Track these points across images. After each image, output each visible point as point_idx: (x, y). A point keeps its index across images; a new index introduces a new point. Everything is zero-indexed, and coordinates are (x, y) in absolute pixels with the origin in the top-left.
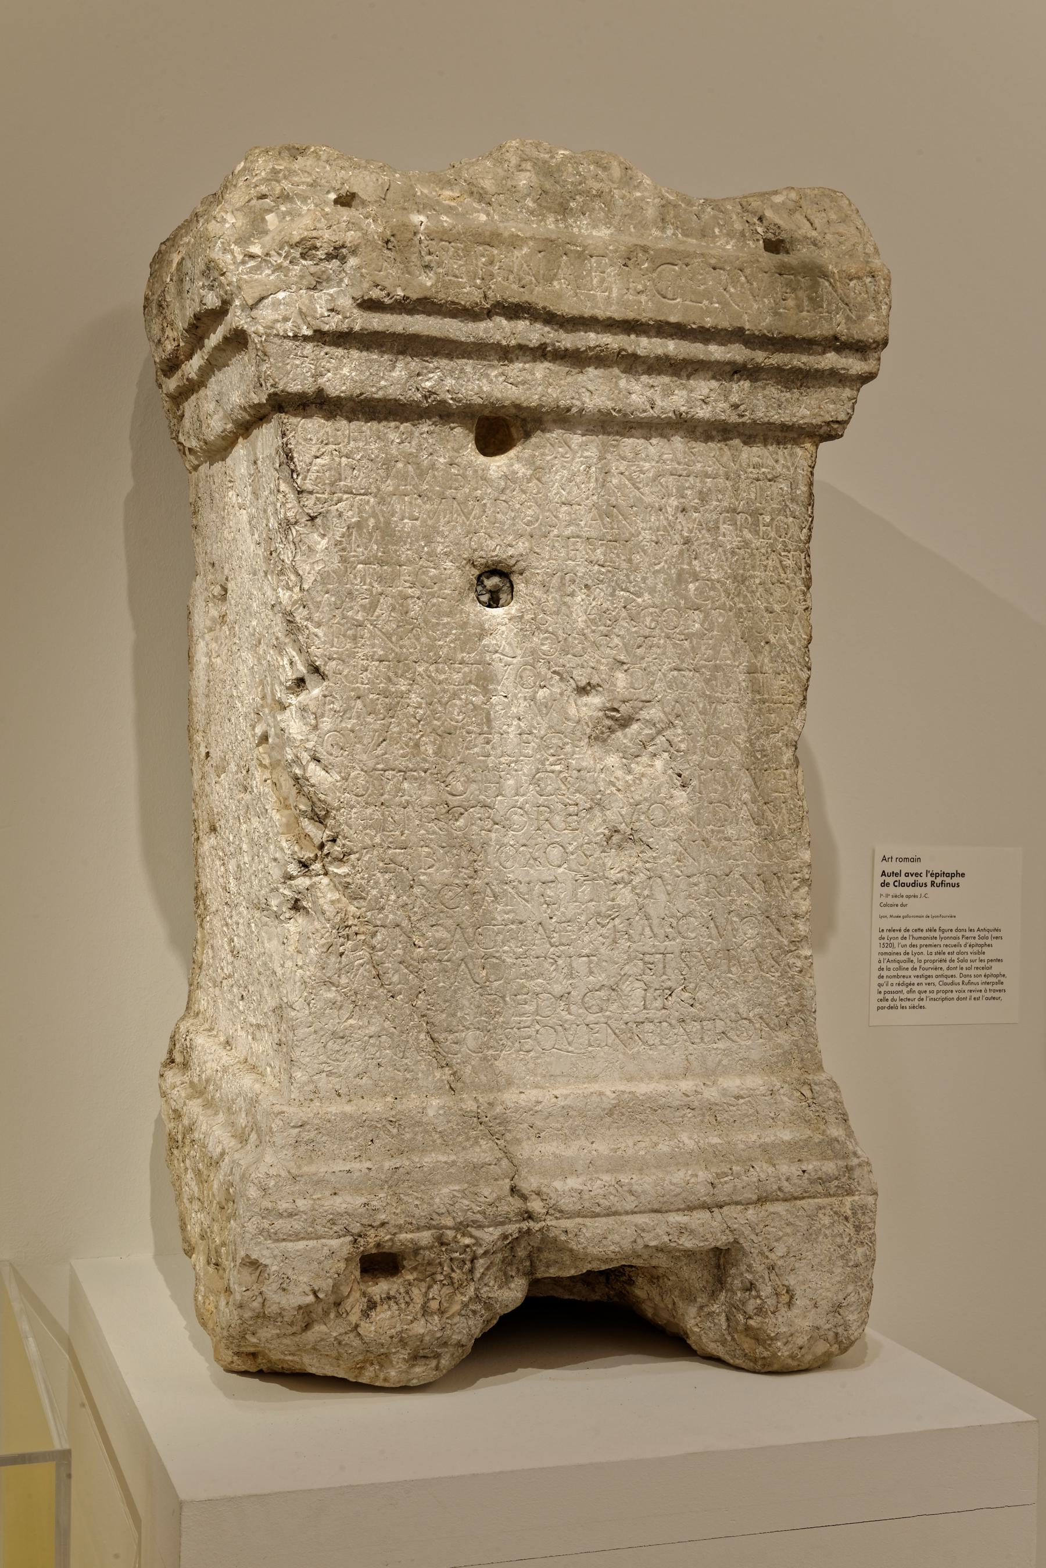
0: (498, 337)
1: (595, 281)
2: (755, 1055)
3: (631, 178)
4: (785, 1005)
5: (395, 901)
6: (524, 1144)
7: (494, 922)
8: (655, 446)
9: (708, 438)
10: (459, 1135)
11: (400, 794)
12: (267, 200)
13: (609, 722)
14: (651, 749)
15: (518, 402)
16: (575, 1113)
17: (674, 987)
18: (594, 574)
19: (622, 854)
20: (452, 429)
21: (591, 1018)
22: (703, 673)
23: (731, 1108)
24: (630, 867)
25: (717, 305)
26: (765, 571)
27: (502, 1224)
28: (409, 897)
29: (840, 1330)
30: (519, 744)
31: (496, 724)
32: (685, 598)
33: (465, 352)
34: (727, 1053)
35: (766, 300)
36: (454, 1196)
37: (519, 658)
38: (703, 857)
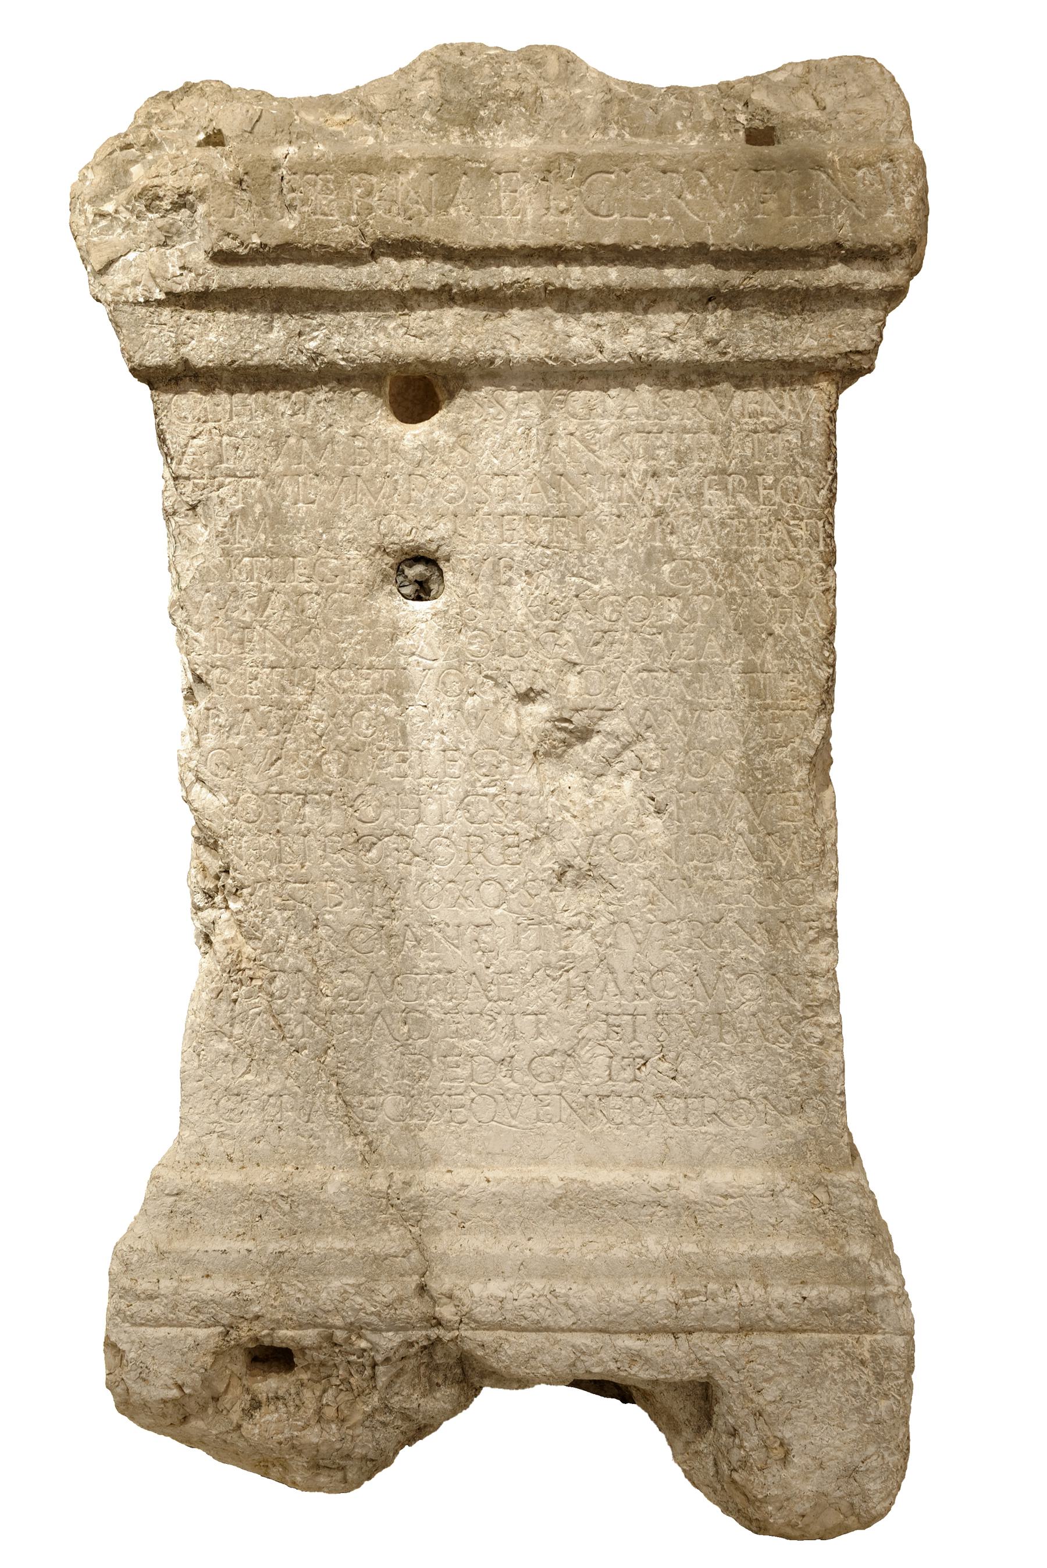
0: (386, 282)
1: (504, 203)
2: (756, 1143)
3: (572, 73)
5: (295, 943)
6: (443, 1234)
7: (416, 970)
8: (614, 399)
9: (685, 384)
10: (364, 1217)
13: (562, 735)
14: (618, 767)
15: (424, 357)
18: (537, 558)
20: (355, 394)
21: (540, 1088)
22: (682, 674)
23: (717, 1209)
24: (589, 909)
25: (668, 218)
26: (768, 545)
27: (404, 1329)
29: (856, 1500)
31: (413, 739)
32: (657, 583)
33: (352, 303)
34: (718, 1138)
35: (737, 206)
36: (346, 1292)
37: (441, 661)
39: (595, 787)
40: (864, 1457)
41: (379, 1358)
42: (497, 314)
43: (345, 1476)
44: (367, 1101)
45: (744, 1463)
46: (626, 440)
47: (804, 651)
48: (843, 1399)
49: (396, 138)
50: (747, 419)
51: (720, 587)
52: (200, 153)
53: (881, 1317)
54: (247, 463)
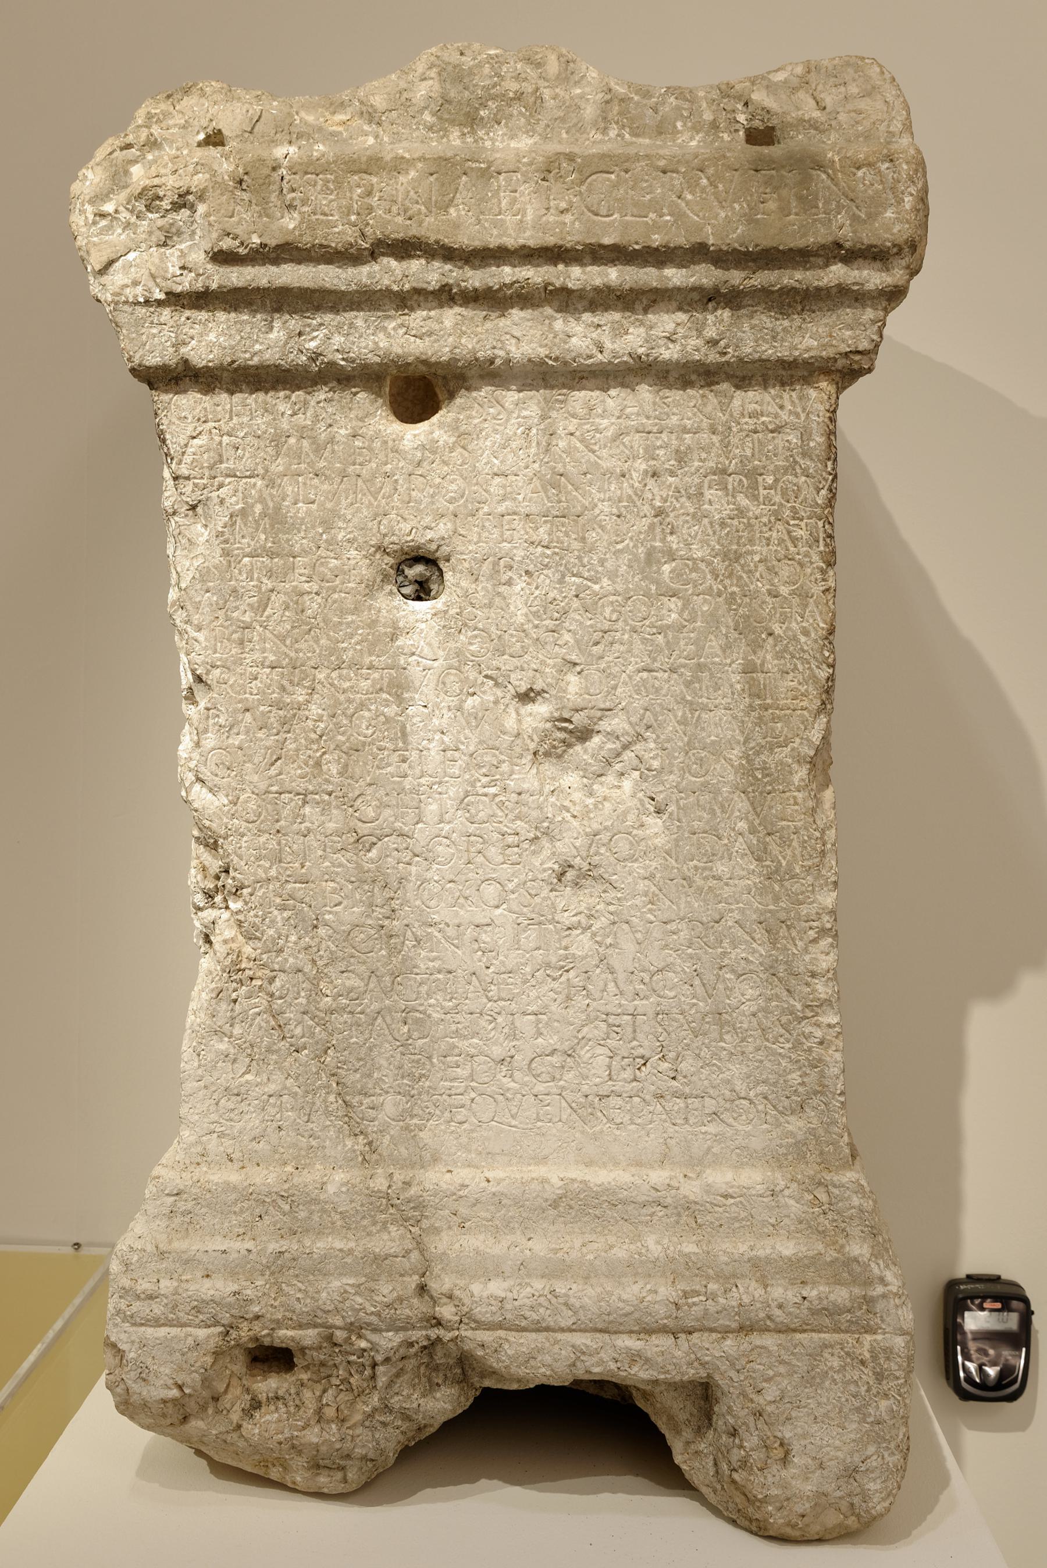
0: (386, 282)
1: (504, 203)
2: (756, 1143)
3: (572, 73)
4: (799, 1084)
5: (295, 943)
7: (416, 970)
8: (614, 399)
9: (685, 384)
10: (364, 1217)
13: (562, 735)
14: (618, 767)
15: (424, 357)
17: (647, 1055)
18: (537, 558)
20: (355, 394)
21: (540, 1088)
22: (682, 674)
23: (717, 1209)
24: (589, 909)
25: (668, 218)
26: (768, 545)
27: (404, 1329)
29: (856, 1500)
31: (413, 739)
32: (657, 583)
33: (352, 303)
34: (718, 1138)
35: (737, 206)
36: (346, 1292)
37: (441, 661)
38: (683, 900)
39: (595, 787)
40: (864, 1457)
41: (379, 1358)
42: (497, 314)
43: (345, 1476)
44: (367, 1101)
45: (744, 1463)
47: (804, 651)
48: (843, 1399)
49: (396, 138)
50: (747, 419)
51: (720, 587)
52: (200, 153)
53: (881, 1317)
54: (247, 463)
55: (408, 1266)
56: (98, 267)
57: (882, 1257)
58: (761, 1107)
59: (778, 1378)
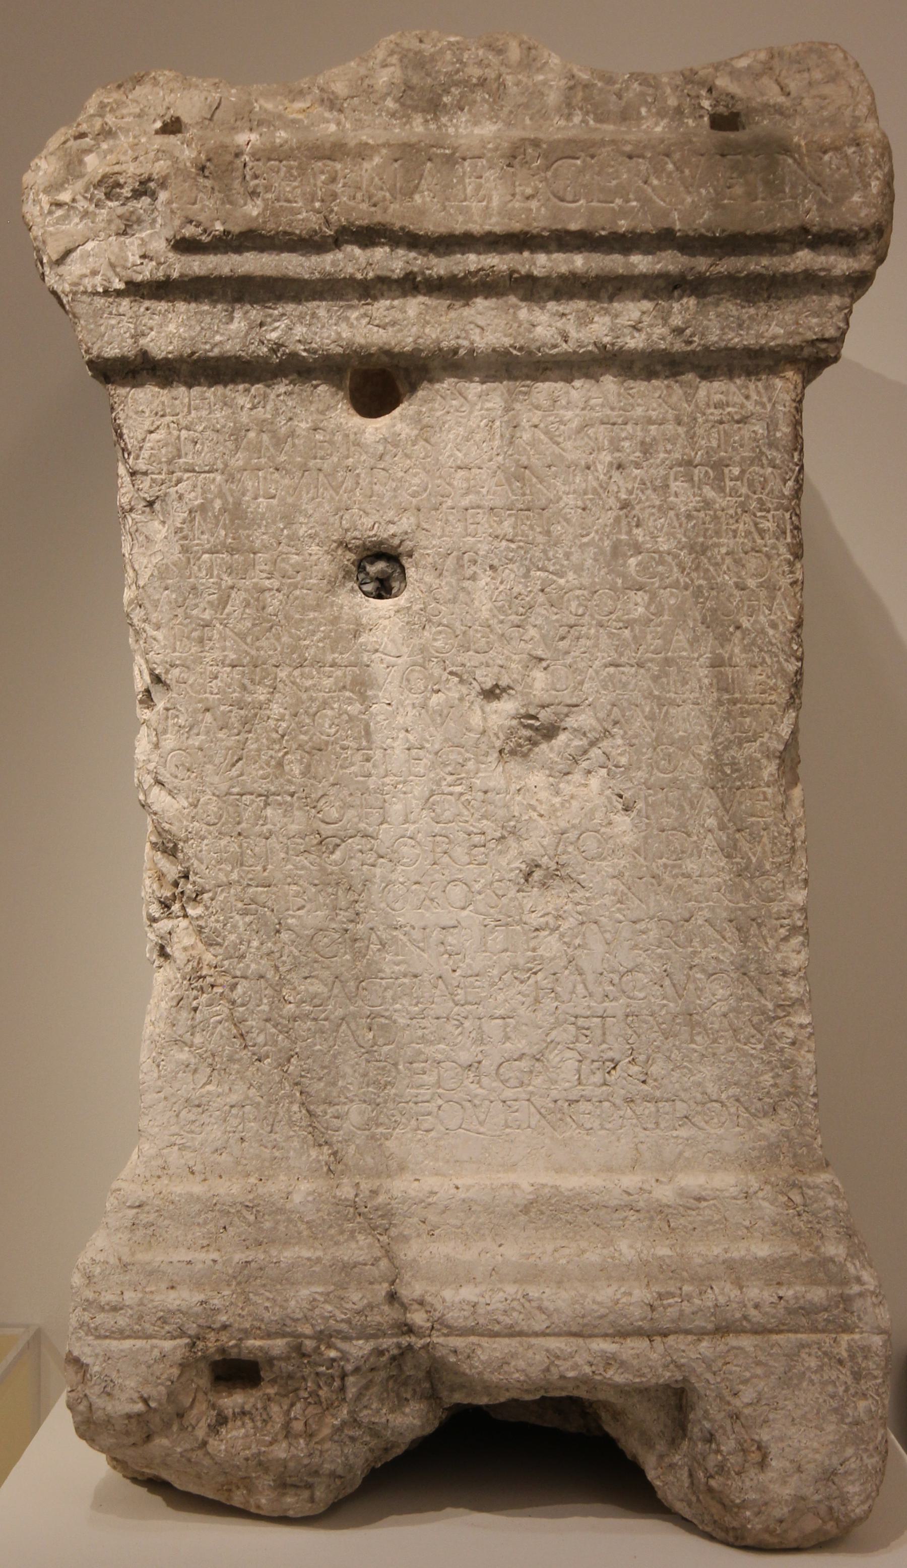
0: (350, 270)
1: (469, 190)
3: (534, 60)
4: (772, 1085)
5: (258, 949)
6: (413, 1242)
7: (380, 975)
9: (650, 374)
10: (331, 1227)
11: (261, 822)
12: (87, 139)
13: (528, 733)
15: (387, 347)
16: (479, 1208)
17: (617, 1058)
18: (501, 552)
19: (549, 894)
20: (316, 387)
21: (509, 1093)
22: (649, 669)
24: (557, 910)
25: (634, 203)
26: (735, 537)
27: (374, 1336)
28: (275, 943)
29: (835, 1504)
30: (407, 761)
31: (377, 738)
32: (624, 576)
35: (703, 191)
36: (314, 1300)
37: (405, 658)
38: (653, 898)
39: (562, 785)
40: (842, 1460)
41: (349, 1367)
42: (461, 303)
44: (331, 1110)
45: (721, 1468)
46: (591, 431)
47: (772, 644)
48: (821, 1400)
49: (359, 124)
50: (712, 410)
51: (687, 580)
53: (859, 1316)
54: (205, 458)
55: (376, 1273)
56: (55, 257)
57: (858, 1258)
58: (733, 1110)
59: (754, 1380)
